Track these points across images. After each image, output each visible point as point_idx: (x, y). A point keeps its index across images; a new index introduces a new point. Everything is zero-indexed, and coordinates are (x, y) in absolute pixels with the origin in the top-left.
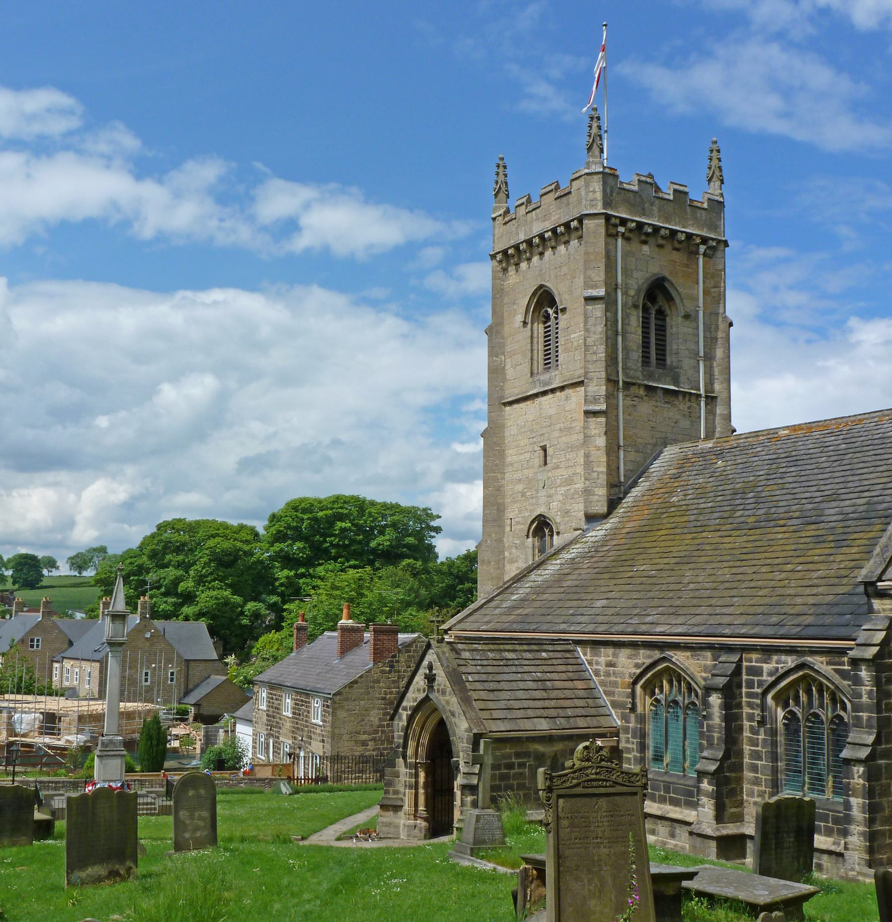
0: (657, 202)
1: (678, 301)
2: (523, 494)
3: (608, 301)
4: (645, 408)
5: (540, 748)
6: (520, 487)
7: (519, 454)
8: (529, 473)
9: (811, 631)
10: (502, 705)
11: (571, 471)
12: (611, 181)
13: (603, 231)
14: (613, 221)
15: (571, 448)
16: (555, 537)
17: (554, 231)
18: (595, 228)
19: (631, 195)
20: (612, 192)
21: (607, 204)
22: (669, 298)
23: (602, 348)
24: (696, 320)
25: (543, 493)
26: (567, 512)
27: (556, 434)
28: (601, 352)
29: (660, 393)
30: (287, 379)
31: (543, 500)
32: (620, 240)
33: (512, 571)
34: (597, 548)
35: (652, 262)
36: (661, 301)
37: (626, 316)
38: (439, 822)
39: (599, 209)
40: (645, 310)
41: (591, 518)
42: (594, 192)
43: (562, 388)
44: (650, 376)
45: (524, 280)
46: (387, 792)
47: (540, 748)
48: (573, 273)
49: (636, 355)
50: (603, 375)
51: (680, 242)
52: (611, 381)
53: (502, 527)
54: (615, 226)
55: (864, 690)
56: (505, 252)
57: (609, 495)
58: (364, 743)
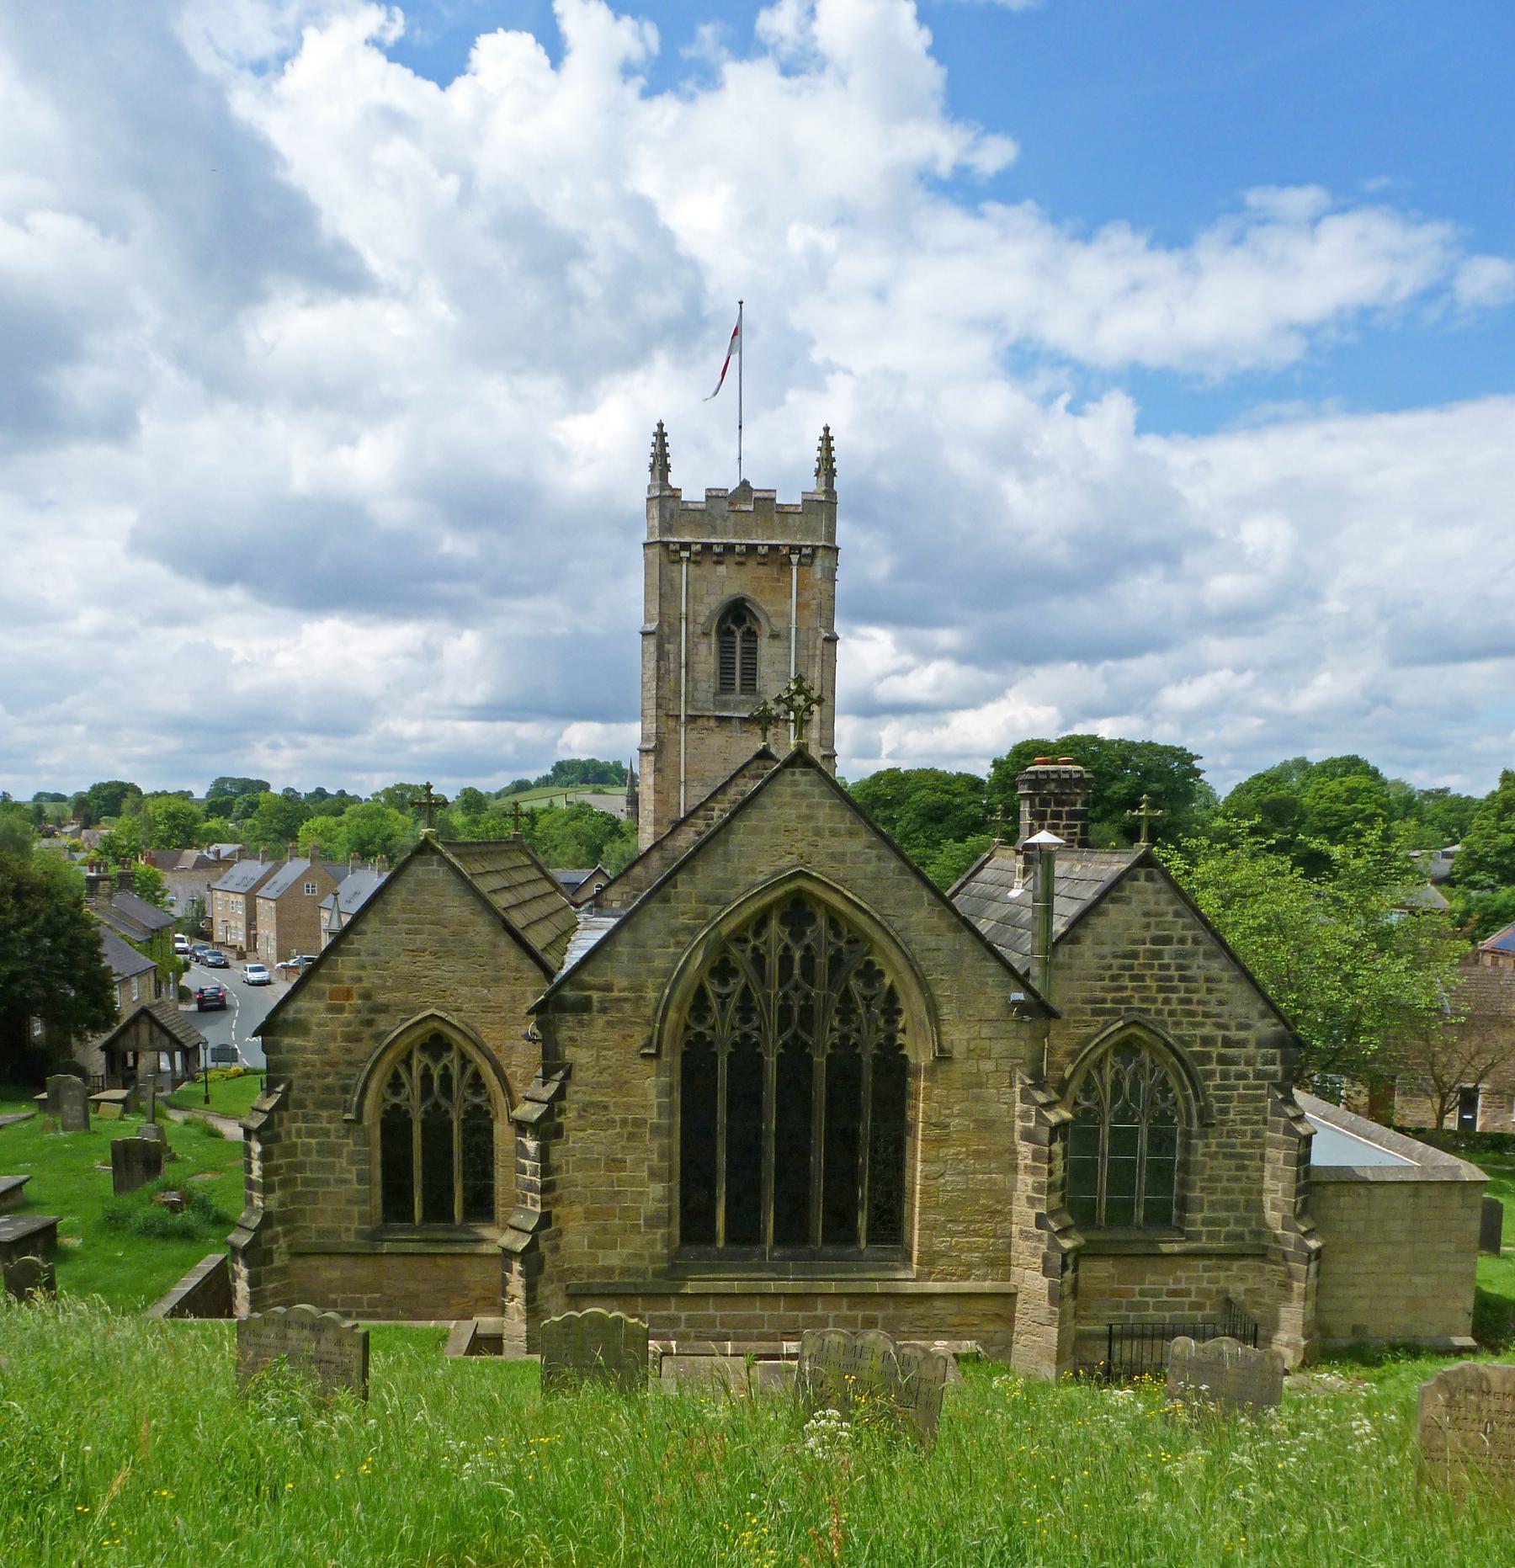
0: (732, 516)
4: (716, 740)
14: (672, 547)
19: (698, 515)
20: (672, 515)
24: (788, 638)
29: (736, 723)
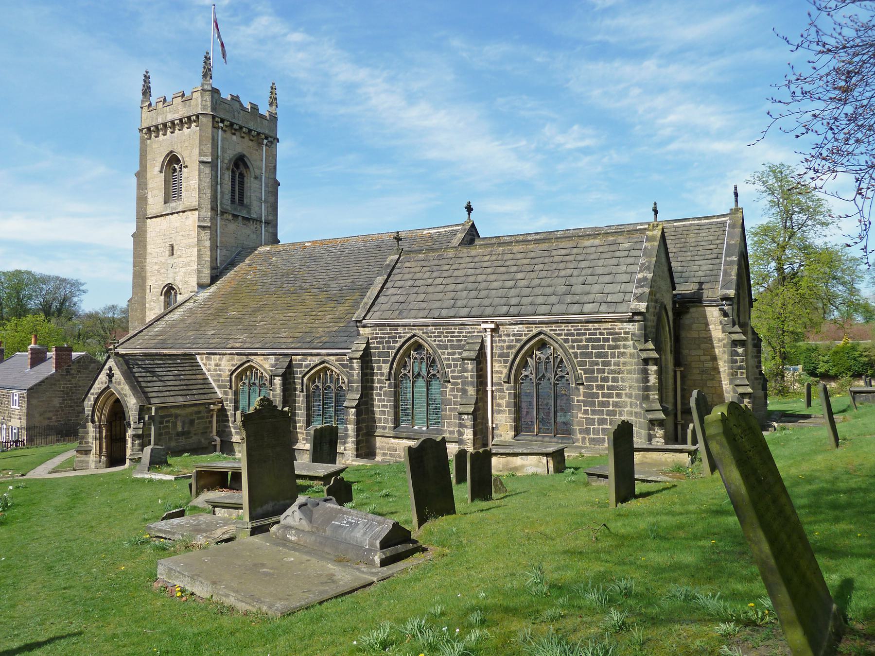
1: (251, 168)
2: (158, 272)
3: (213, 165)
4: (232, 226)
5: (178, 411)
6: (156, 267)
7: (155, 248)
8: (163, 259)
9: (327, 345)
10: (156, 389)
11: (188, 259)
12: (216, 95)
13: (211, 124)
14: (217, 119)
15: (189, 246)
16: (178, 296)
17: (181, 120)
18: (207, 122)
21: (213, 109)
22: (246, 166)
23: (209, 191)
25: (171, 271)
26: (186, 282)
27: (180, 238)
28: (208, 192)
29: (240, 218)
30: (823, 224)
31: (171, 275)
32: (220, 131)
33: (150, 316)
34: (205, 301)
35: (237, 145)
36: (242, 168)
37: (222, 174)
38: (116, 458)
39: (209, 111)
40: (233, 172)
41: (202, 286)
42: (206, 101)
43: (184, 212)
44: (235, 209)
45: (161, 146)
46: (80, 443)
47: (178, 411)
48: (190, 145)
49: (228, 197)
50: (209, 206)
51: (253, 136)
52: (213, 209)
53: (144, 290)
54: (218, 122)
55: (355, 372)
56: (149, 129)
57: (211, 273)
58: (49, 419)
